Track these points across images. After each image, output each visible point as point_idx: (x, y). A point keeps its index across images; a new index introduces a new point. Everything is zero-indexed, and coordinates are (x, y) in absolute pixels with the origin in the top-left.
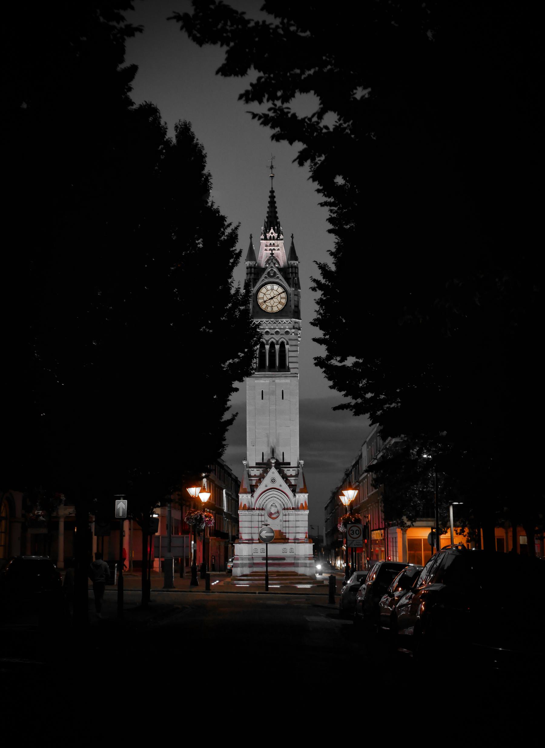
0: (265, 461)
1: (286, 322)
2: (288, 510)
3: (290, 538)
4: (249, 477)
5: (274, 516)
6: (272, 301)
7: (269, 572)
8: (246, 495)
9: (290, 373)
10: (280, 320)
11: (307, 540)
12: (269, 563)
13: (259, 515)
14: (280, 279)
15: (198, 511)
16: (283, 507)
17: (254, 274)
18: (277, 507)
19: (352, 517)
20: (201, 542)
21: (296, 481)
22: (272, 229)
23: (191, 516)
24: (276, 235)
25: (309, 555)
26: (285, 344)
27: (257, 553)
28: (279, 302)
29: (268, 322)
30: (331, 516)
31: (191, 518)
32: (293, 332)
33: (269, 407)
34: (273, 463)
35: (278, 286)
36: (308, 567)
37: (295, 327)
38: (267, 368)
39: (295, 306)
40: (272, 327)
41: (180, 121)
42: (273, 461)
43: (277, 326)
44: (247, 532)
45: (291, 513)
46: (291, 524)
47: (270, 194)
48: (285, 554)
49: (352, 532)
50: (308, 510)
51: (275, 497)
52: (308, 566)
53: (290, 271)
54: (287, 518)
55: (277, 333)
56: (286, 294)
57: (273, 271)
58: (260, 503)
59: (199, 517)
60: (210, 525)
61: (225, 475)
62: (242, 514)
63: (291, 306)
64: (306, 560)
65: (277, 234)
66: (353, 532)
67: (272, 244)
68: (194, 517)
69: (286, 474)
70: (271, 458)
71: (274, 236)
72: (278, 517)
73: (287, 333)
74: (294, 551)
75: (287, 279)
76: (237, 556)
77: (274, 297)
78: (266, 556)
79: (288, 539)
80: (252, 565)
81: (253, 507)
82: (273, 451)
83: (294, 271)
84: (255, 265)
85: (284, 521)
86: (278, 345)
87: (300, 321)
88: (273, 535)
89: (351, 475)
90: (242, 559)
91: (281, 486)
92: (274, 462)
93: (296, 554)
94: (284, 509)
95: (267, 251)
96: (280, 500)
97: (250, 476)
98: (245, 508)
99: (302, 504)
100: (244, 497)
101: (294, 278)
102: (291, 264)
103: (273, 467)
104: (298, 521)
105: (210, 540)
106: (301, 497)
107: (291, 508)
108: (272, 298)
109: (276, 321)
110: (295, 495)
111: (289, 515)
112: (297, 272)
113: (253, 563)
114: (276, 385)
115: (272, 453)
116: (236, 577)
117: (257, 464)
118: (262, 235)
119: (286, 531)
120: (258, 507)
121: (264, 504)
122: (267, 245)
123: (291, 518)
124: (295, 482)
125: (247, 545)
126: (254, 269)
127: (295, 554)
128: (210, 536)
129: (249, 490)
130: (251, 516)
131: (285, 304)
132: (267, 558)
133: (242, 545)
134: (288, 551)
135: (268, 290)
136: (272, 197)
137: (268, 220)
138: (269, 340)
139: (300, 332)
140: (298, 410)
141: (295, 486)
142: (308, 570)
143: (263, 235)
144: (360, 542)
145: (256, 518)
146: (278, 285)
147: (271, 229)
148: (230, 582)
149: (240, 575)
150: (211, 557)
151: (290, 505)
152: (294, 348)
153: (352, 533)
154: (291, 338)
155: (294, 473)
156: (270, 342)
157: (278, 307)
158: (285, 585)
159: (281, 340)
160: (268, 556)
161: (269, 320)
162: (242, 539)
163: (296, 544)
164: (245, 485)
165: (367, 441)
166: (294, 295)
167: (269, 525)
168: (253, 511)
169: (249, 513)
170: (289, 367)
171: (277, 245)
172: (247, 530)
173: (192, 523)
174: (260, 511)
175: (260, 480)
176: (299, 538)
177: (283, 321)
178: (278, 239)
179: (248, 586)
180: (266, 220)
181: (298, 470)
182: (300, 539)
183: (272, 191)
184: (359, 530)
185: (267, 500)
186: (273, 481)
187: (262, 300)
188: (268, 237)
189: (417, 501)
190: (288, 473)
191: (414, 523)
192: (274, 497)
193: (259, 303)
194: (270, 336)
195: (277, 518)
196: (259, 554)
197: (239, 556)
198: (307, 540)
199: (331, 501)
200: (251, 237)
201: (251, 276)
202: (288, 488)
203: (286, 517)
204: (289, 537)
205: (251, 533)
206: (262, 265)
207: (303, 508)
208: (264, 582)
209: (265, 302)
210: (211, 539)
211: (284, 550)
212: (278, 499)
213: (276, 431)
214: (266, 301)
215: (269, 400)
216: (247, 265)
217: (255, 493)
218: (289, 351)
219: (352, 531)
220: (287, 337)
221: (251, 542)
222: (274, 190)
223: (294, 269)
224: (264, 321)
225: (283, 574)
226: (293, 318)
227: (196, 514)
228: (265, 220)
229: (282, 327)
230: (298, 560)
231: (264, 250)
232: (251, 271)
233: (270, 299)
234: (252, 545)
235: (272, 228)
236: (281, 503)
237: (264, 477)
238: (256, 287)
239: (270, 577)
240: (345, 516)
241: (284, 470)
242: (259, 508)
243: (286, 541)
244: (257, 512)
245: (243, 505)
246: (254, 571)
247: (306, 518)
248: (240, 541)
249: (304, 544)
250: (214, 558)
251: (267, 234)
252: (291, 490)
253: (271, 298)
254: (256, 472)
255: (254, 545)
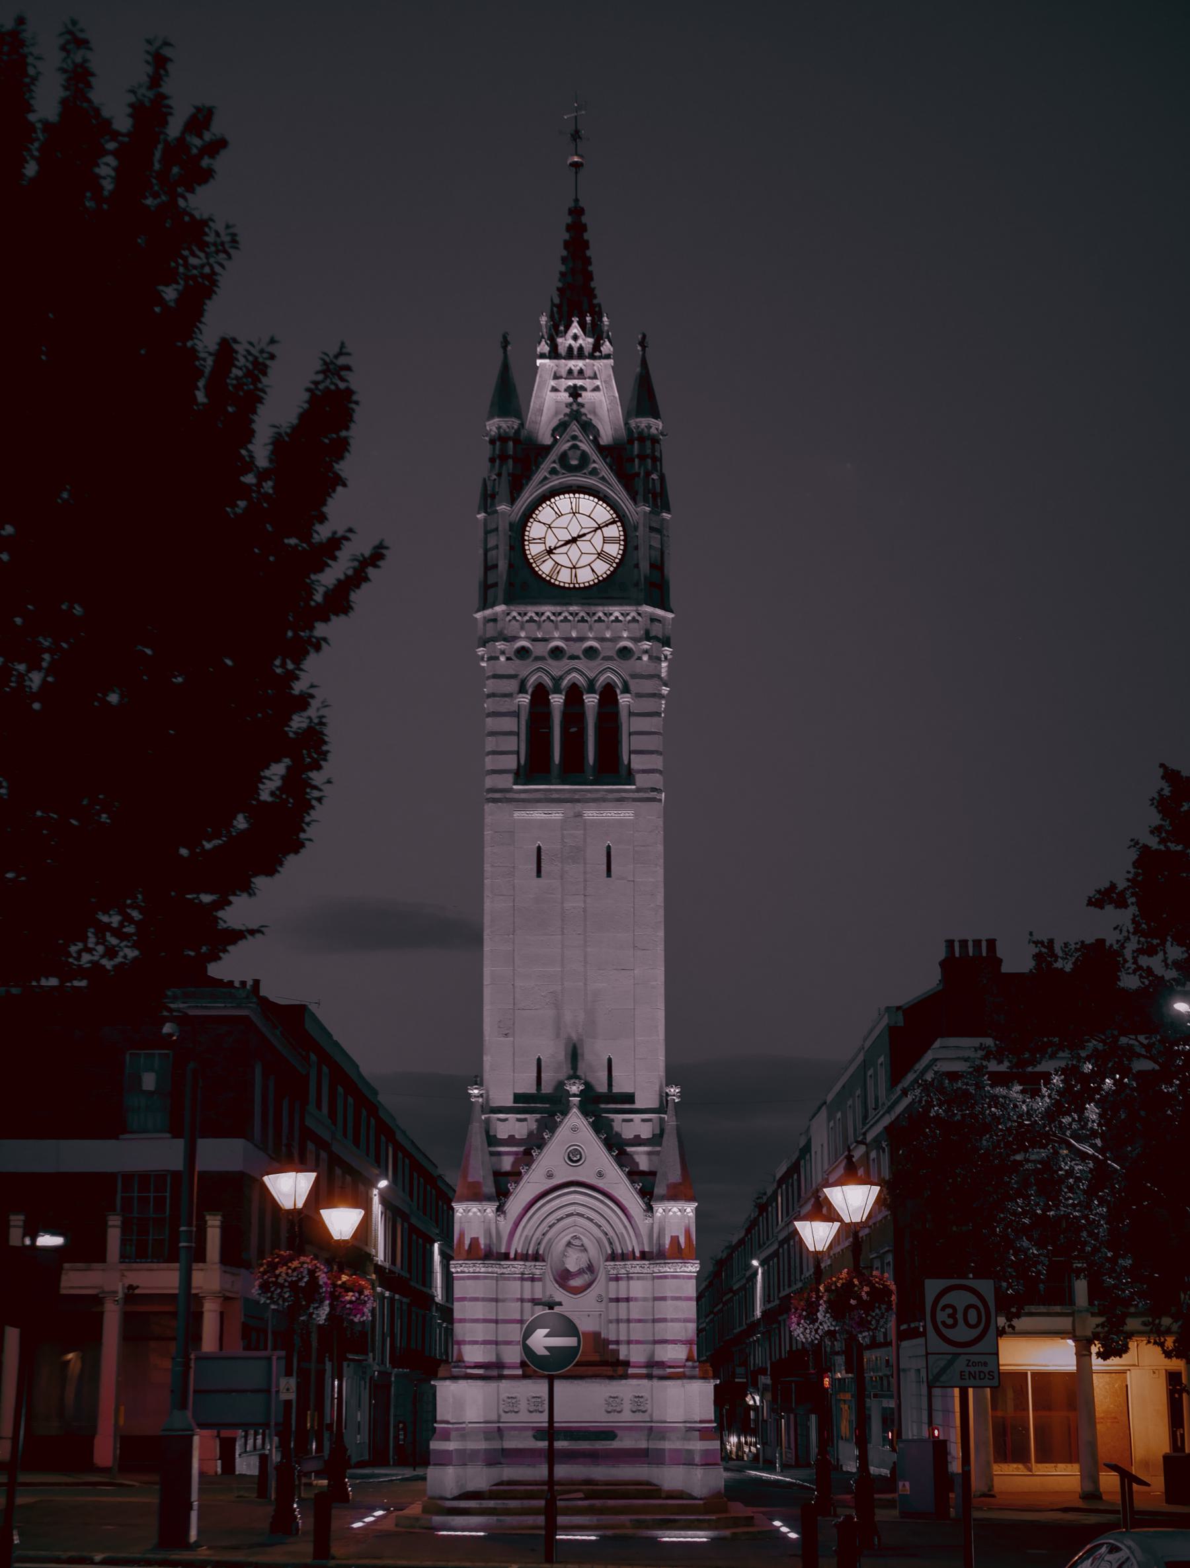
0: (547, 1088)
1: (621, 618)
2: (628, 1260)
3: (633, 1359)
4: (490, 1145)
5: (576, 1282)
6: (573, 550)
7: (560, 1483)
8: (480, 1207)
9: (634, 787)
10: (600, 608)
11: (694, 1367)
12: (559, 1450)
13: (522, 1279)
14: (603, 479)
15: (302, 1259)
16: (609, 1252)
17: (516, 460)
18: (585, 1250)
19: (860, 1283)
20: (365, 1382)
21: (654, 1158)
22: (575, 324)
23: (277, 1276)
24: (587, 342)
25: (701, 1422)
26: (618, 692)
27: (517, 1412)
28: (599, 554)
29: (561, 618)
30: (712, 1321)
31: (276, 1284)
32: (646, 652)
33: (562, 903)
34: (575, 1095)
35: (596, 500)
36: (697, 1465)
37: (653, 634)
38: (555, 771)
39: (652, 566)
40: (574, 634)
41: (344, 350)
42: (575, 1089)
43: (591, 629)
44: (480, 1339)
45: (638, 1269)
46: (636, 1310)
47: (569, 220)
48: (614, 1417)
49: (949, 1316)
50: (696, 1259)
51: (582, 1215)
52: (697, 1460)
53: (636, 452)
54: (622, 1289)
55: (591, 653)
56: (623, 526)
57: (579, 452)
58: (527, 1236)
59: (305, 1280)
60: (359, 1316)
61: (440, 1203)
62: (462, 1272)
63: (637, 566)
64: (689, 1440)
65: (591, 340)
66: (952, 1316)
67: (576, 370)
68: (286, 1280)
69: (618, 1135)
70: (570, 1078)
71: (583, 345)
72: (589, 1285)
73: (625, 653)
74: (648, 1407)
75: (627, 480)
76: (446, 1426)
77: (580, 536)
78: (546, 1425)
79: (627, 1364)
80: (495, 1458)
81: (503, 1251)
82: (574, 1055)
83: (649, 451)
84: (517, 432)
85: (611, 1300)
86: (595, 693)
87: (670, 615)
88: (575, 1344)
89: (774, 1204)
90: (464, 1435)
91: (600, 1175)
92: (578, 1093)
93: (655, 1418)
94: (613, 1257)
95: (558, 394)
96: (599, 1227)
97: (492, 1140)
98: (475, 1253)
99: (675, 1240)
100: (470, 1214)
101: (648, 474)
102: (638, 427)
103: (575, 1110)
104: (663, 1299)
105: (393, 1379)
106: (671, 1213)
107: (637, 1254)
108: (574, 540)
109: (588, 614)
110: (650, 1209)
111: (629, 1278)
112: (657, 454)
113: (503, 1450)
114: (585, 829)
115: (569, 1061)
116: (440, 1502)
117: (518, 1098)
118: (543, 343)
119: (618, 1335)
120: (519, 1251)
121: (542, 1240)
122: (558, 375)
123: (637, 1289)
124: (650, 1160)
125: (480, 1383)
126: (514, 444)
127: (651, 1416)
128: (393, 1367)
129: (489, 1188)
130: (495, 1281)
131: (617, 561)
132: (550, 1432)
133: (462, 1384)
134: (627, 1406)
135: (560, 515)
136: (577, 228)
137: (561, 301)
138: (561, 678)
139: (668, 653)
140: (661, 912)
141: (650, 1178)
142: (699, 1476)
143: (547, 344)
144: (985, 1364)
145: (514, 1289)
146: (595, 496)
147: (572, 322)
148: (417, 1519)
149: (456, 1493)
150: (396, 1426)
151: (632, 1244)
152: (648, 705)
153: (950, 1321)
154: (638, 671)
155: (646, 1132)
156: (565, 683)
157: (593, 571)
158: (617, 1531)
159: (602, 679)
160: (555, 1425)
161: (564, 608)
162: (464, 1362)
163: (656, 1382)
164: (479, 1171)
165: (828, 1102)
166: (648, 529)
167: (560, 1304)
168: (502, 1263)
169: (490, 1270)
170: (632, 766)
171: (592, 375)
172: (479, 1332)
173: (280, 1302)
174: (527, 1264)
175: (527, 1153)
176: (665, 1359)
177: (611, 614)
178: (595, 353)
179: (482, 1534)
180: (557, 301)
181: (662, 1120)
182: (669, 1364)
183: (576, 207)
184: (980, 1304)
185: (551, 1227)
186: (575, 1157)
187: (541, 548)
188: (562, 350)
189: (1029, 1249)
190: (628, 1132)
191: (1015, 1322)
192: (578, 1214)
193: (529, 557)
194: (565, 664)
195: (586, 1290)
196: (524, 1417)
197: (450, 1426)
198: (694, 1367)
199: (709, 1282)
200: (505, 343)
201: (504, 467)
202: (628, 1183)
203: (618, 1285)
204: (628, 1355)
205: (497, 1343)
206: (540, 437)
207: (677, 1252)
208: (541, 1520)
209: (550, 552)
210: (396, 1376)
211: (613, 1404)
212: (591, 1220)
213: (585, 984)
214: (555, 548)
215: (562, 877)
216: (493, 433)
217: (511, 1198)
218: (631, 714)
219: (949, 1311)
220: (625, 668)
221: (495, 1373)
222: (582, 204)
223: (648, 443)
224: (548, 614)
225: (607, 1490)
226: (647, 604)
227: (294, 1270)
228: (552, 300)
229: (608, 635)
230: (663, 1438)
231: (550, 388)
232: (503, 449)
233: (567, 543)
234: (498, 1386)
235: (575, 319)
236: (601, 1235)
237: (541, 1145)
238: (521, 503)
239: (560, 1500)
240: (834, 1279)
241: (613, 1120)
242: (525, 1252)
243: (620, 1370)
244: (518, 1267)
245: (467, 1242)
246: (505, 1478)
247: (690, 1289)
248: (455, 1371)
249: (685, 1381)
250: (404, 1429)
251: (560, 340)
252: (636, 1189)
253: (570, 538)
254: (512, 1127)
255: (504, 1384)
